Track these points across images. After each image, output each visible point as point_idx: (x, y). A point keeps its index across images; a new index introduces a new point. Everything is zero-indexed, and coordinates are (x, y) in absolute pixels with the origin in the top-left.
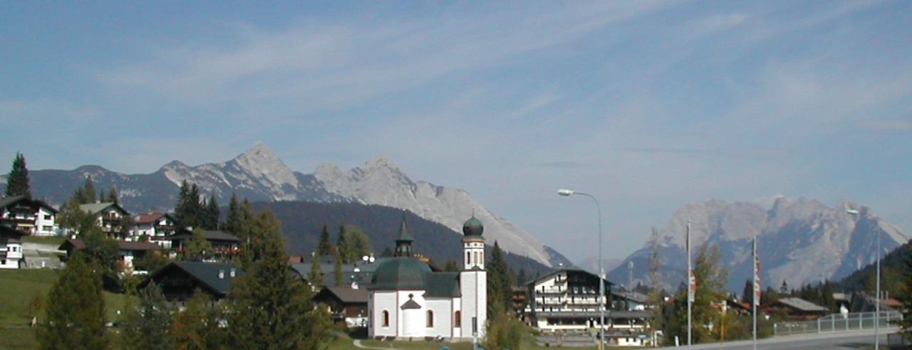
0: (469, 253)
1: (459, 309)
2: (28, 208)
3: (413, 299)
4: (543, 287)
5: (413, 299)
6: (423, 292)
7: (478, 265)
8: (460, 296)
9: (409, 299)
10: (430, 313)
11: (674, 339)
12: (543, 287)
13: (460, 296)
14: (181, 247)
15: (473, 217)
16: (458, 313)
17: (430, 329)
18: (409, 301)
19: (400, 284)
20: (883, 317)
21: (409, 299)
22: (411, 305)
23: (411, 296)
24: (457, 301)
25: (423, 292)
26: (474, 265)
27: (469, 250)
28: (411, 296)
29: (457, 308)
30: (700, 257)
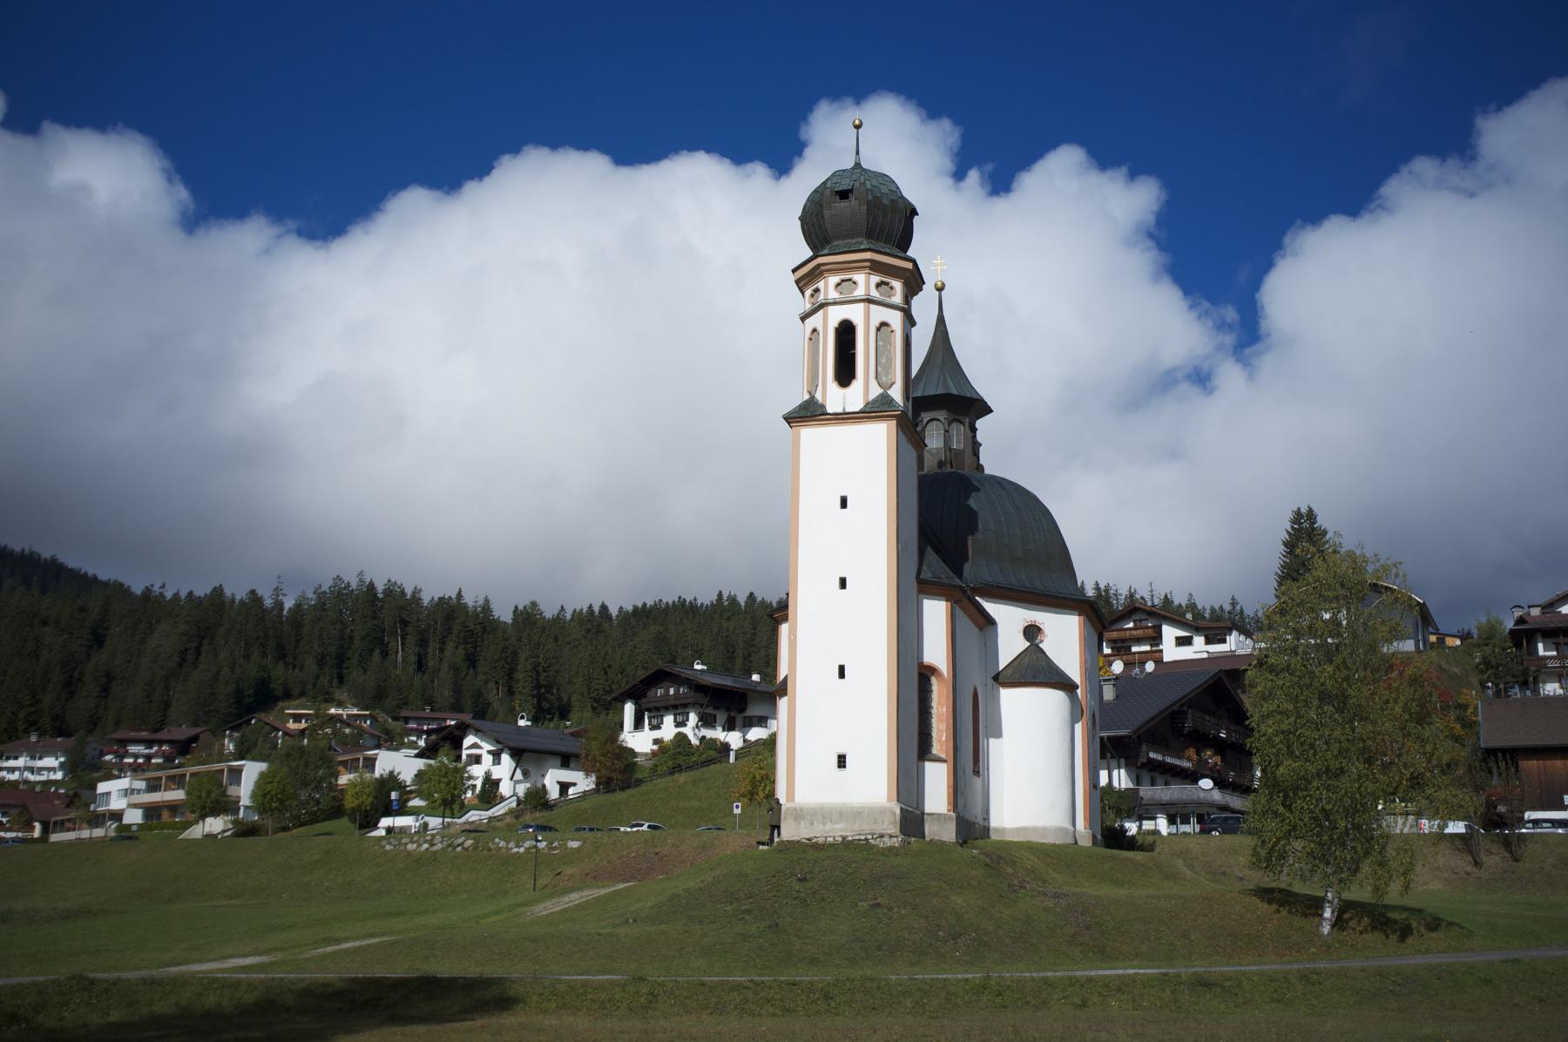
0: (846, 333)
26: (875, 391)
28: (1032, 632)
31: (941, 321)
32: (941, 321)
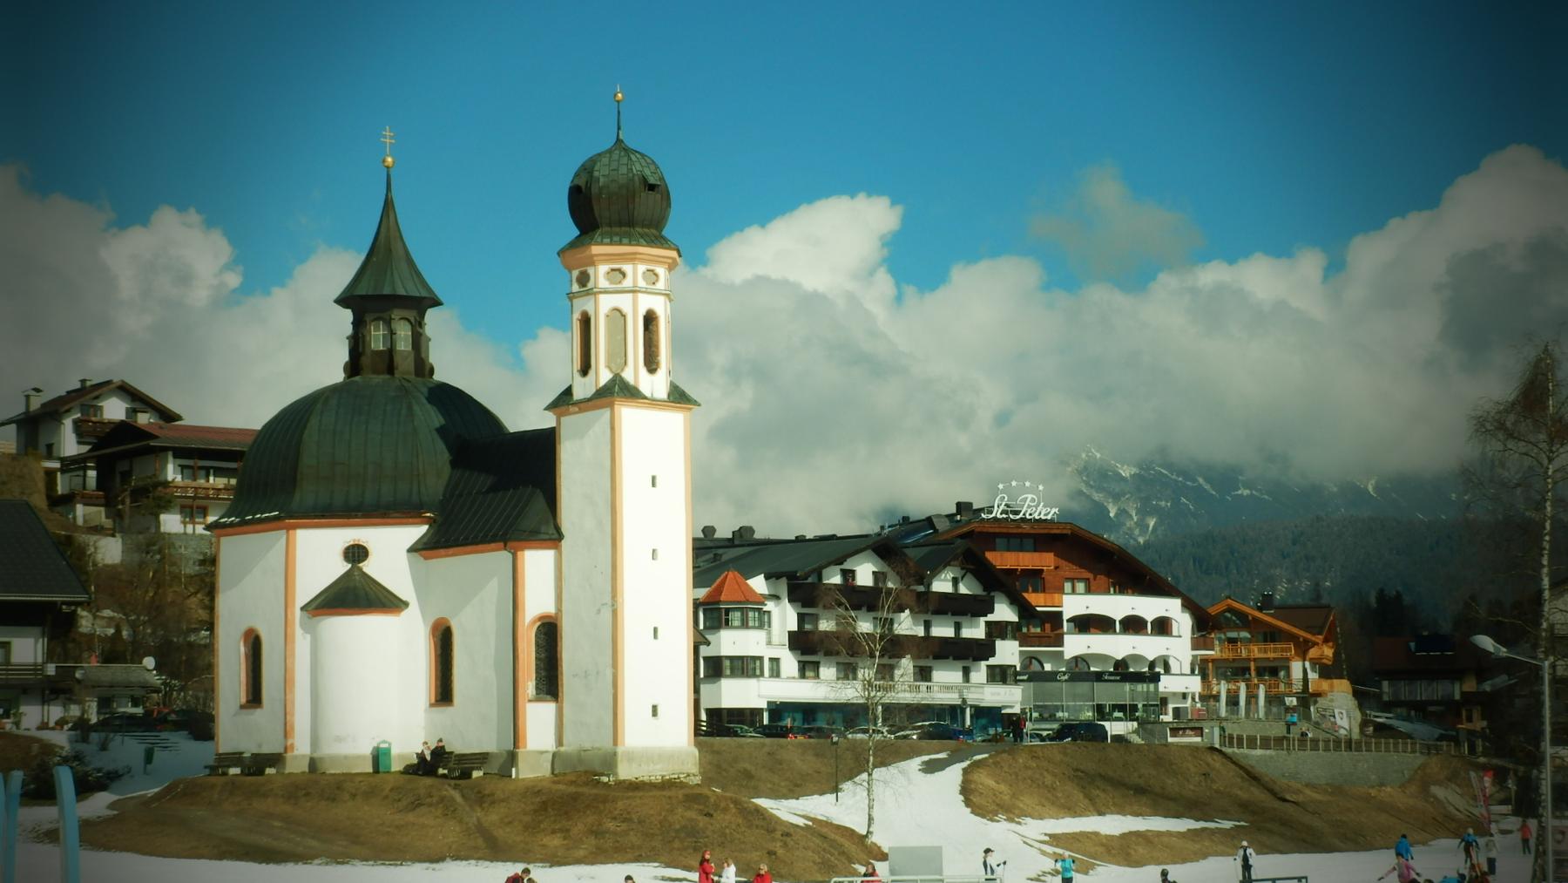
1: (550, 609)
2: (1245, 634)
3: (369, 567)
5: (369, 567)
6: (416, 532)
7: (628, 375)
8: (553, 537)
10: (443, 640)
11: (760, 812)
13: (553, 537)
14: (810, 580)
15: (618, 140)
16: (549, 632)
17: (445, 712)
18: (347, 576)
19: (306, 493)
20: (1321, 744)
22: (355, 594)
23: (356, 554)
24: (537, 563)
25: (416, 532)
26: (605, 377)
27: (624, 302)
28: (356, 554)
29: (538, 601)
30: (1540, 360)
31: (388, 205)
32: (388, 205)
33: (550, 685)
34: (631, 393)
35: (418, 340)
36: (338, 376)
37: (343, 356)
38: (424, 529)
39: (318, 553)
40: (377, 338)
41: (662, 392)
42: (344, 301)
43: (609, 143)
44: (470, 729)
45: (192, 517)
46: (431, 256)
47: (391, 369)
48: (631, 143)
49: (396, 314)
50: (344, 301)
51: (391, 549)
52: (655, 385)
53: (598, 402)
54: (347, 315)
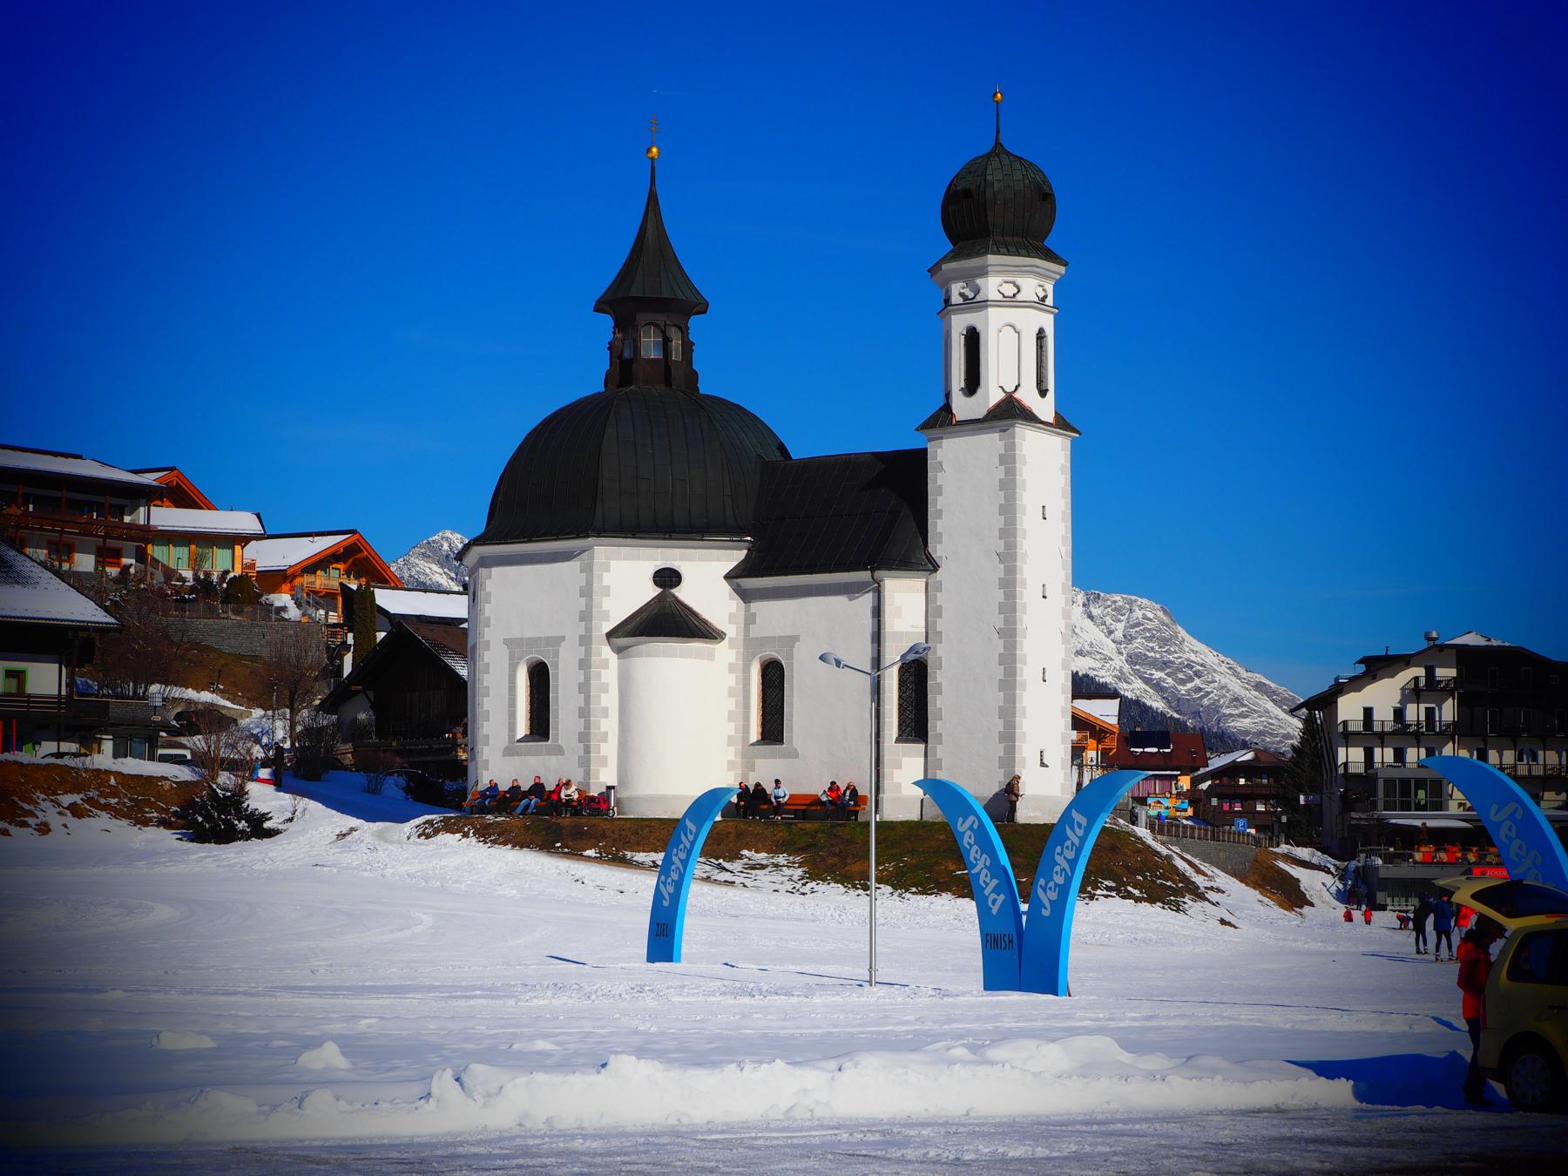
3: (683, 593)
4: (1368, 712)
5: (683, 593)
9: (652, 591)
10: (773, 677)
12: (1368, 712)
16: (916, 674)
21: (652, 591)
22: (666, 620)
23: (667, 578)
24: (904, 596)
25: (733, 557)
28: (667, 578)
31: (652, 199)
32: (652, 199)
33: (916, 725)
34: (1029, 417)
35: (688, 347)
36: (599, 387)
37: (603, 363)
38: (741, 555)
39: (624, 575)
40: (650, 347)
41: (1050, 418)
42: (601, 306)
43: (986, 147)
44: (799, 773)
45: (57, 552)
46: (697, 255)
47: (668, 381)
48: (1009, 145)
49: (642, 318)
50: (601, 306)
51: (706, 576)
52: (1045, 408)
53: (986, 425)
54: (607, 321)
